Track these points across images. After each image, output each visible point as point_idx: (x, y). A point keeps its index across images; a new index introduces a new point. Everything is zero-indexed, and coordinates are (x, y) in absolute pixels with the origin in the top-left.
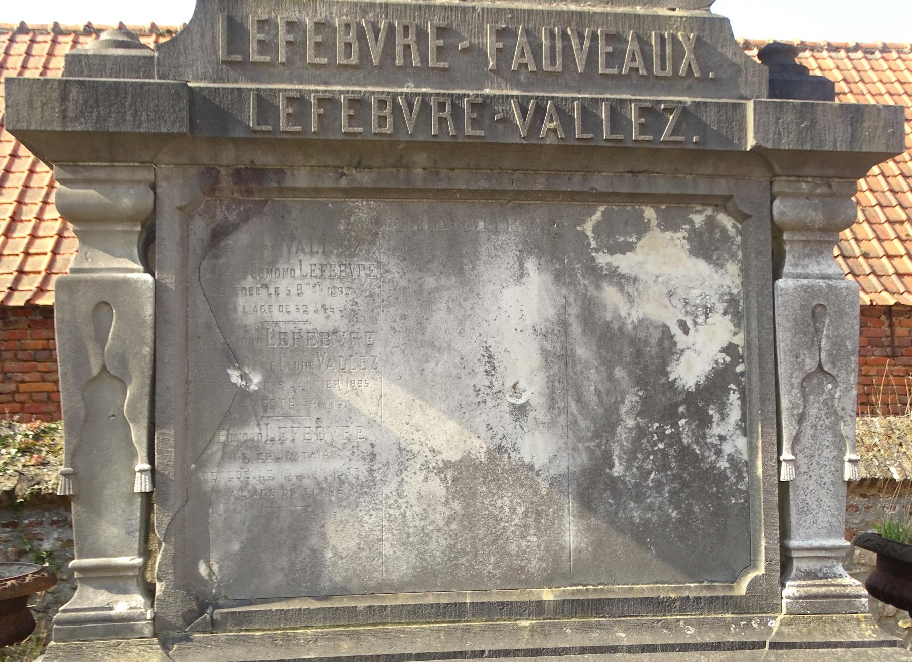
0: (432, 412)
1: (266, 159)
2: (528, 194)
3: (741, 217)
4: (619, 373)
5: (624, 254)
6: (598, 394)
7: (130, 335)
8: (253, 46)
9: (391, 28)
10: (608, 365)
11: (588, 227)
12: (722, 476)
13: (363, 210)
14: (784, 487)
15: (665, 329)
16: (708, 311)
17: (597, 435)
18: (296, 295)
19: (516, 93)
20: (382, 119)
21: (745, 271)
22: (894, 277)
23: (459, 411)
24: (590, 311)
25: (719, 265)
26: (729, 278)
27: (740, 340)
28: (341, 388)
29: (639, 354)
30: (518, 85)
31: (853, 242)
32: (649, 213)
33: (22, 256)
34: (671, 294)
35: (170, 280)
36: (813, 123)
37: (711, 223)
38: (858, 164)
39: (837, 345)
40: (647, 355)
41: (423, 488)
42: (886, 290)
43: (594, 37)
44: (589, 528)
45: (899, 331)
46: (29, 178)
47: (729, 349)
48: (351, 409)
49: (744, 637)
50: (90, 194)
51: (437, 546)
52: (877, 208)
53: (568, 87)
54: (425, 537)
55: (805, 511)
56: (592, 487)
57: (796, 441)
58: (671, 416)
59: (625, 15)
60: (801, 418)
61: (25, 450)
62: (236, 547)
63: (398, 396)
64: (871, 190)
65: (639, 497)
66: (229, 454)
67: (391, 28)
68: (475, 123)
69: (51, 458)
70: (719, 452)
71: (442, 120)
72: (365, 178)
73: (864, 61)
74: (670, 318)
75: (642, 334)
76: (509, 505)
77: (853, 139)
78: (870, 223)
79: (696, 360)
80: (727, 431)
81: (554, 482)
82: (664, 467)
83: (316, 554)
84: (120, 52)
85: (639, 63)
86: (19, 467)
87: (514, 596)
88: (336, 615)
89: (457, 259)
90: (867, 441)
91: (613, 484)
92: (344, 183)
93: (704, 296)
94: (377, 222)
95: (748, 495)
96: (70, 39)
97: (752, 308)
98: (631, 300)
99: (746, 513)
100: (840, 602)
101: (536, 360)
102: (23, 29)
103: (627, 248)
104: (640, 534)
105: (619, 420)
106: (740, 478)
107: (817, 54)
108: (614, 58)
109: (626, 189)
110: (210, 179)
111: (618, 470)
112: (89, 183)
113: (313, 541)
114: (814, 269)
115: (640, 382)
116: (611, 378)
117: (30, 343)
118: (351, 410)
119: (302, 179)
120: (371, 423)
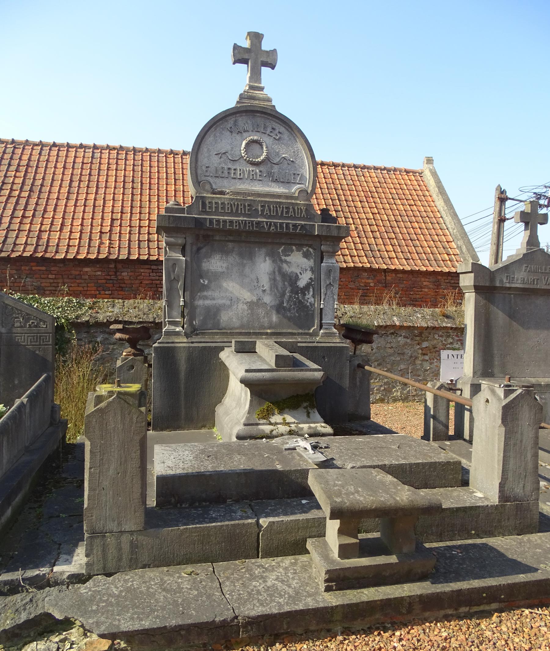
0: (245, 290)
1: (210, 233)
2: (268, 243)
3: (314, 249)
4: (286, 283)
6: (281, 288)
7: (180, 271)
8: (207, 208)
9: (238, 204)
10: (284, 281)
11: (280, 251)
12: (308, 307)
13: (230, 245)
14: (321, 309)
15: (297, 274)
16: (306, 270)
17: (281, 297)
18: (215, 264)
19: (265, 220)
20: (236, 226)
21: (315, 261)
22: (388, 259)
23: (250, 291)
24: (280, 269)
25: (309, 260)
26: (311, 263)
27: (313, 277)
28: (225, 284)
29: (291, 279)
30: (266, 218)
31: (375, 245)
32: (294, 248)
33: (68, 239)
34: (298, 266)
35: (188, 259)
36: (330, 229)
37: (308, 250)
38: (339, 239)
39: (334, 278)
40: (292, 280)
41: (242, 307)
42: (384, 263)
43: (283, 207)
44: (278, 317)
45: (388, 278)
46: (65, 208)
47: (311, 279)
48: (227, 289)
49: (311, 341)
50: (172, 240)
51: (245, 319)
52: (385, 233)
53: (276, 219)
54: (242, 318)
55: (326, 315)
56: (279, 308)
57: (324, 299)
58: (297, 293)
59: (290, 203)
60: (326, 294)
61: (90, 308)
62: (202, 318)
63: (237, 287)
64: (384, 226)
65: (289, 311)
66: (200, 298)
67: (238, 204)
68: (256, 227)
69: (99, 311)
70: (307, 301)
71: (249, 226)
72: (231, 238)
73: (387, 175)
75: (291, 275)
76: (261, 312)
77: (338, 233)
78: (382, 238)
79: (304, 280)
80: (309, 297)
81: (271, 307)
82: (295, 304)
83: (219, 320)
84: (176, 207)
85: (293, 214)
86: (90, 313)
87: (262, 331)
88: (223, 333)
89: (251, 256)
90: (368, 313)
91: (284, 308)
92: (227, 239)
93: (305, 267)
94: (234, 248)
95: (313, 311)
96: (74, 149)
97: (316, 270)
98: (289, 267)
99: (313, 315)
100: (332, 335)
101: (268, 280)
102: (54, 145)
103: (289, 255)
104: (289, 319)
105: (286, 294)
106: (312, 307)
107: (369, 171)
108: (287, 212)
109: (289, 242)
110: (197, 237)
111: (285, 305)
112: (171, 237)
113: (218, 318)
114: (330, 261)
115: (291, 285)
116: (284, 284)
117: (73, 272)
118: (227, 290)
119: (217, 238)
120: (231, 292)
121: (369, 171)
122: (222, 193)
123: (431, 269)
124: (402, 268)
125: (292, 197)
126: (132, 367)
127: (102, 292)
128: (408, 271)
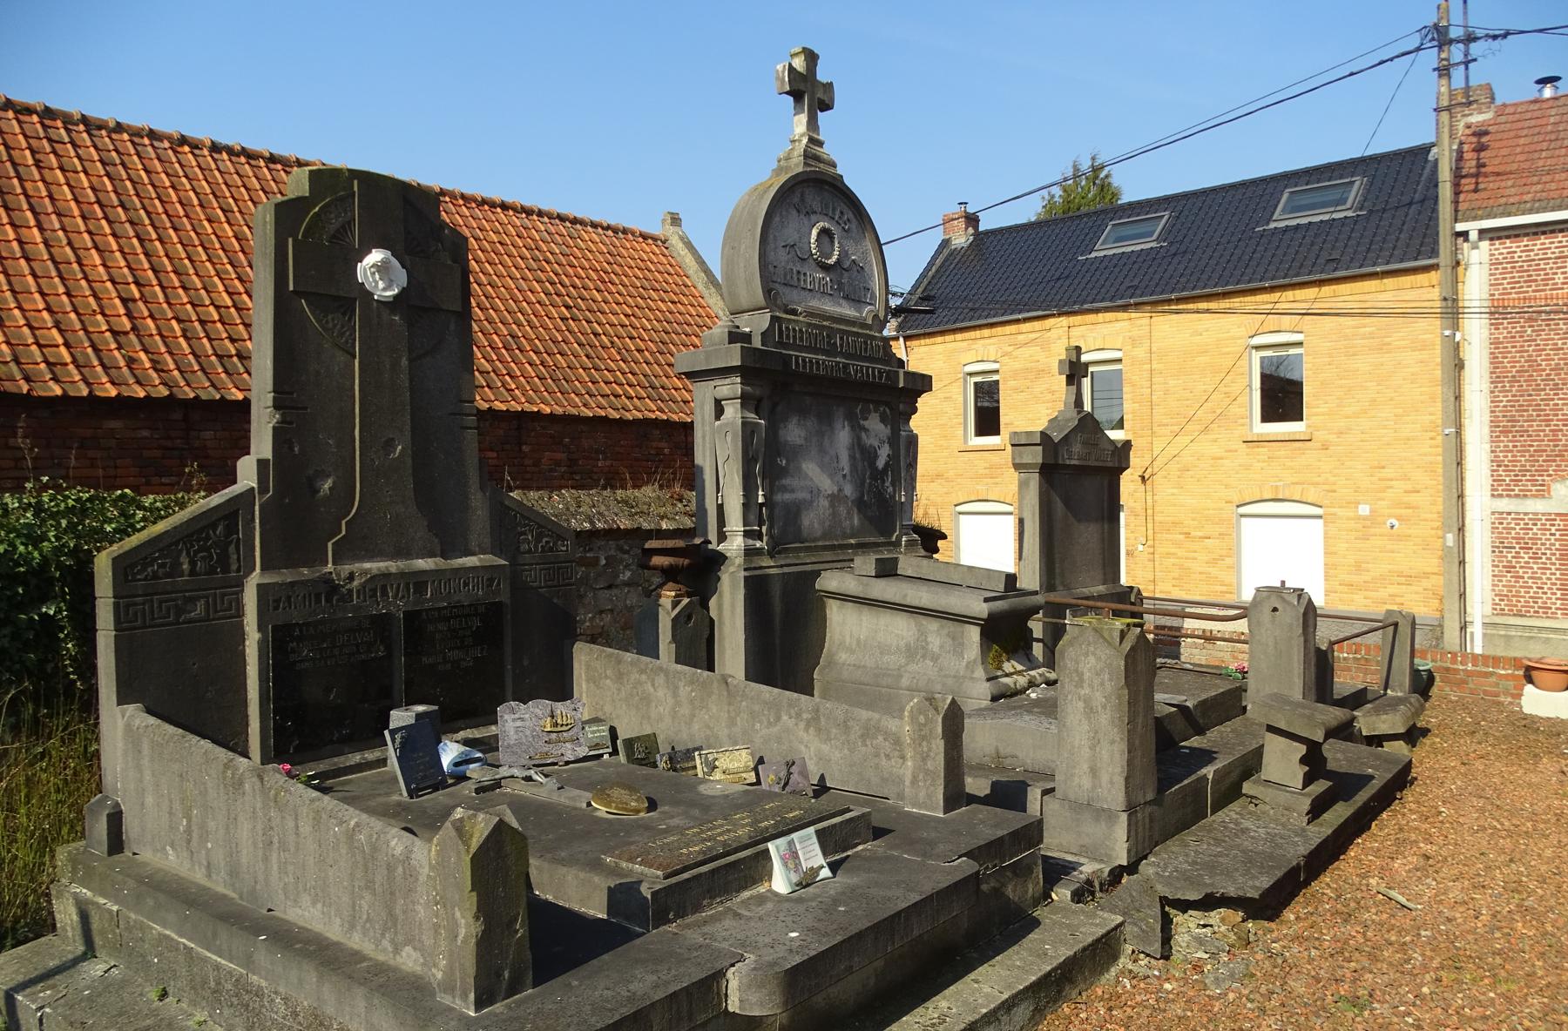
5: (915, 410)
23: (831, 476)
63: (818, 470)
74: (876, 444)
76: (842, 510)
88: (808, 549)
121: (136, 140)
122: (794, 312)
123: (559, 410)
124: (192, 395)
125: (864, 325)
126: (689, 618)
127: (155, 480)
128: (615, 420)
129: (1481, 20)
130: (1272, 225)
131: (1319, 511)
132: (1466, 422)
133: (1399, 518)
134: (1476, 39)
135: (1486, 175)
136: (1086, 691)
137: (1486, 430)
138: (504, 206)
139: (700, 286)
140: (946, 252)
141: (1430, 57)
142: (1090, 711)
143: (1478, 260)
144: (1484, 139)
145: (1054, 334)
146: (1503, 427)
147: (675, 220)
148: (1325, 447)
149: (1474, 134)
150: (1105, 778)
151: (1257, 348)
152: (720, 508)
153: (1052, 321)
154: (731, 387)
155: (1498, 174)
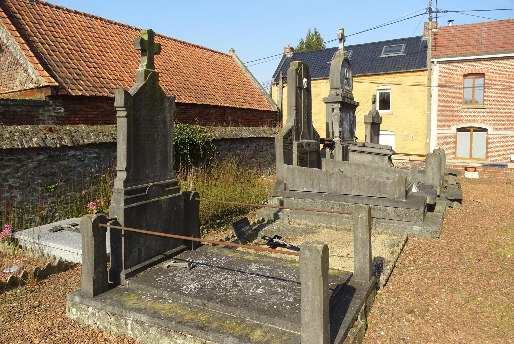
129: (441, 8)
130: (381, 56)
131: (394, 133)
132: (432, 110)
133: (414, 135)
134: (440, 12)
135: (437, 46)
136: (432, 165)
137: (436, 113)
138: (197, 47)
139: (244, 71)
140: (285, 59)
141: (427, 16)
142: (433, 169)
143: (436, 69)
144: (436, 36)
145: (322, 84)
146: (441, 112)
147: (234, 51)
148: (396, 117)
149: (434, 35)
150: (435, 180)
151: (378, 90)
152: (333, 131)
153: (321, 81)
154: (339, 105)
155: (440, 46)
